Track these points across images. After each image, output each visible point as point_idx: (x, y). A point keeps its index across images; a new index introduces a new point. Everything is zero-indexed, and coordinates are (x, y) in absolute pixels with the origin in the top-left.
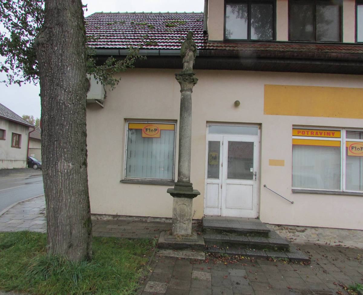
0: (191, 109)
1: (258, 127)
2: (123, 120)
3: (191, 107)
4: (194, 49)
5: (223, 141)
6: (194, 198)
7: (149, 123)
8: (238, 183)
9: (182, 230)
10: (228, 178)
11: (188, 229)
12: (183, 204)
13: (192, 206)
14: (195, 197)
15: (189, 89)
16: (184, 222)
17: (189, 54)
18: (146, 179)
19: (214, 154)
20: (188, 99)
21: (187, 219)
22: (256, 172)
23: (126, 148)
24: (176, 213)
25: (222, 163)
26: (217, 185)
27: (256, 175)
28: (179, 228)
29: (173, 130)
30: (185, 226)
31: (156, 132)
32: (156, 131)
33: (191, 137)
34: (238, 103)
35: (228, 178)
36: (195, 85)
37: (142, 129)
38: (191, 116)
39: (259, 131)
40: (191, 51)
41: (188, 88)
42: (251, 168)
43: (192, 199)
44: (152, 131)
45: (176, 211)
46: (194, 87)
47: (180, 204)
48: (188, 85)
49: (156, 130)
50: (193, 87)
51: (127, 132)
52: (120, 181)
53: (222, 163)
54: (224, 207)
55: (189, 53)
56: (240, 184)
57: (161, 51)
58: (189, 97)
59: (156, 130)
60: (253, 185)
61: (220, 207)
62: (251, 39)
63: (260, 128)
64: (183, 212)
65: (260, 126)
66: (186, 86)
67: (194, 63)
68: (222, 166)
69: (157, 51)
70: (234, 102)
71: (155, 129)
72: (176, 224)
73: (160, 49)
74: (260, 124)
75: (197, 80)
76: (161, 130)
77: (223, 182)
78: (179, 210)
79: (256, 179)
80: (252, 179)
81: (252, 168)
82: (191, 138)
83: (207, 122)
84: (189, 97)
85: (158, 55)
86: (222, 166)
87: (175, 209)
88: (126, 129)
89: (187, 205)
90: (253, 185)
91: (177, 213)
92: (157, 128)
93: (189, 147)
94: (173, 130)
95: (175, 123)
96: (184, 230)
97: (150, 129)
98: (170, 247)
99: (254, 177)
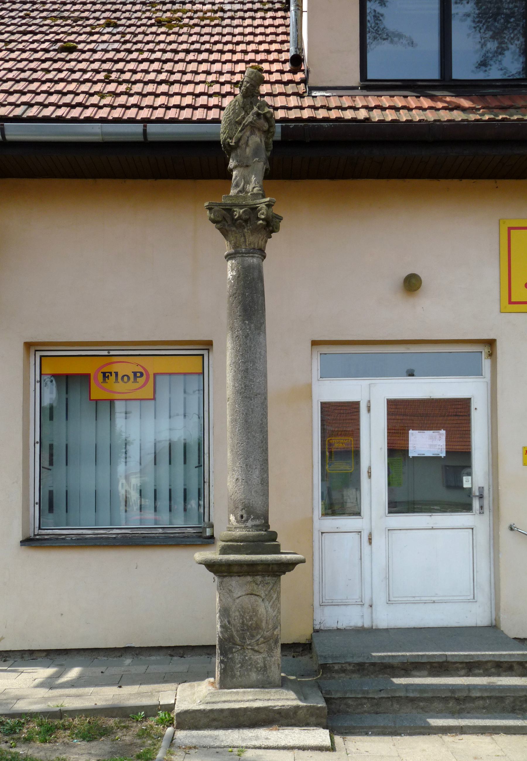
0: (264, 310)
1: (485, 350)
2: (20, 349)
3: (263, 305)
4: (266, 126)
5: (369, 402)
6: (284, 573)
7: (112, 353)
8: (208, 435)
9: (251, 670)
10: (390, 512)
11: (270, 667)
12: (252, 594)
13: (278, 598)
14: (290, 571)
15: (254, 249)
16: (256, 648)
17: (250, 142)
18: (111, 532)
19: (339, 443)
20: (253, 279)
21: (265, 638)
22: (481, 489)
23: (34, 435)
24: (229, 622)
25: (370, 468)
26: (356, 536)
27: (481, 497)
28: (241, 667)
29: (199, 374)
30: (258, 658)
31: (141, 380)
32: (138, 379)
33: (266, 393)
34: (413, 281)
35: (390, 512)
36: (273, 235)
37: (88, 375)
38: (265, 333)
39: (486, 363)
40: (257, 132)
41: (252, 246)
42: (465, 478)
43: (280, 576)
44: (126, 378)
45: (229, 616)
46: (269, 240)
47: (240, 594)
48: (251, 238)
49: (138, 375)
50: (266, 242)
51: (38, 385)
52: (21, 542)
53: (370, 468)
54: (380, 600)
55: (248, 137)
56: (432, 529)
57: (152, 128)
58: (256, 274)
59: (138, 375)
60: (472, 529)
61: (367, 603)
62: (455, 76)
63: (492, 355)
64: (251, 618)
65: (492, 349)
66: (245, 241)
67: (266, 170)
68: (370, 477)
69: (138, 128)
70: (402, 280)
71: (135, 373)
72: (230, 656)
73: (146, 121)
74: (491, 343)
75: (281, 219)
76: (155, 375)
77: (373, 528)
78: (237, 614)
79: (482, 507)
80: (467, 507)
81: (470, 477)
82: (266, 399)
83: (315, 343)
84: (256, 274)
85: (141, 138)
86: (369, 410)
87: (225, 612)
88: (34, 374)
89: (263, 595)
90: (472, 529)
91: (233, 622)
92: (141, 370)
93: (262, 424)
94: (199, 374)
95: (205, 353)
96: (258, 671)
97: (117, 374)
98: (215, 723)
99: (476, 504)
